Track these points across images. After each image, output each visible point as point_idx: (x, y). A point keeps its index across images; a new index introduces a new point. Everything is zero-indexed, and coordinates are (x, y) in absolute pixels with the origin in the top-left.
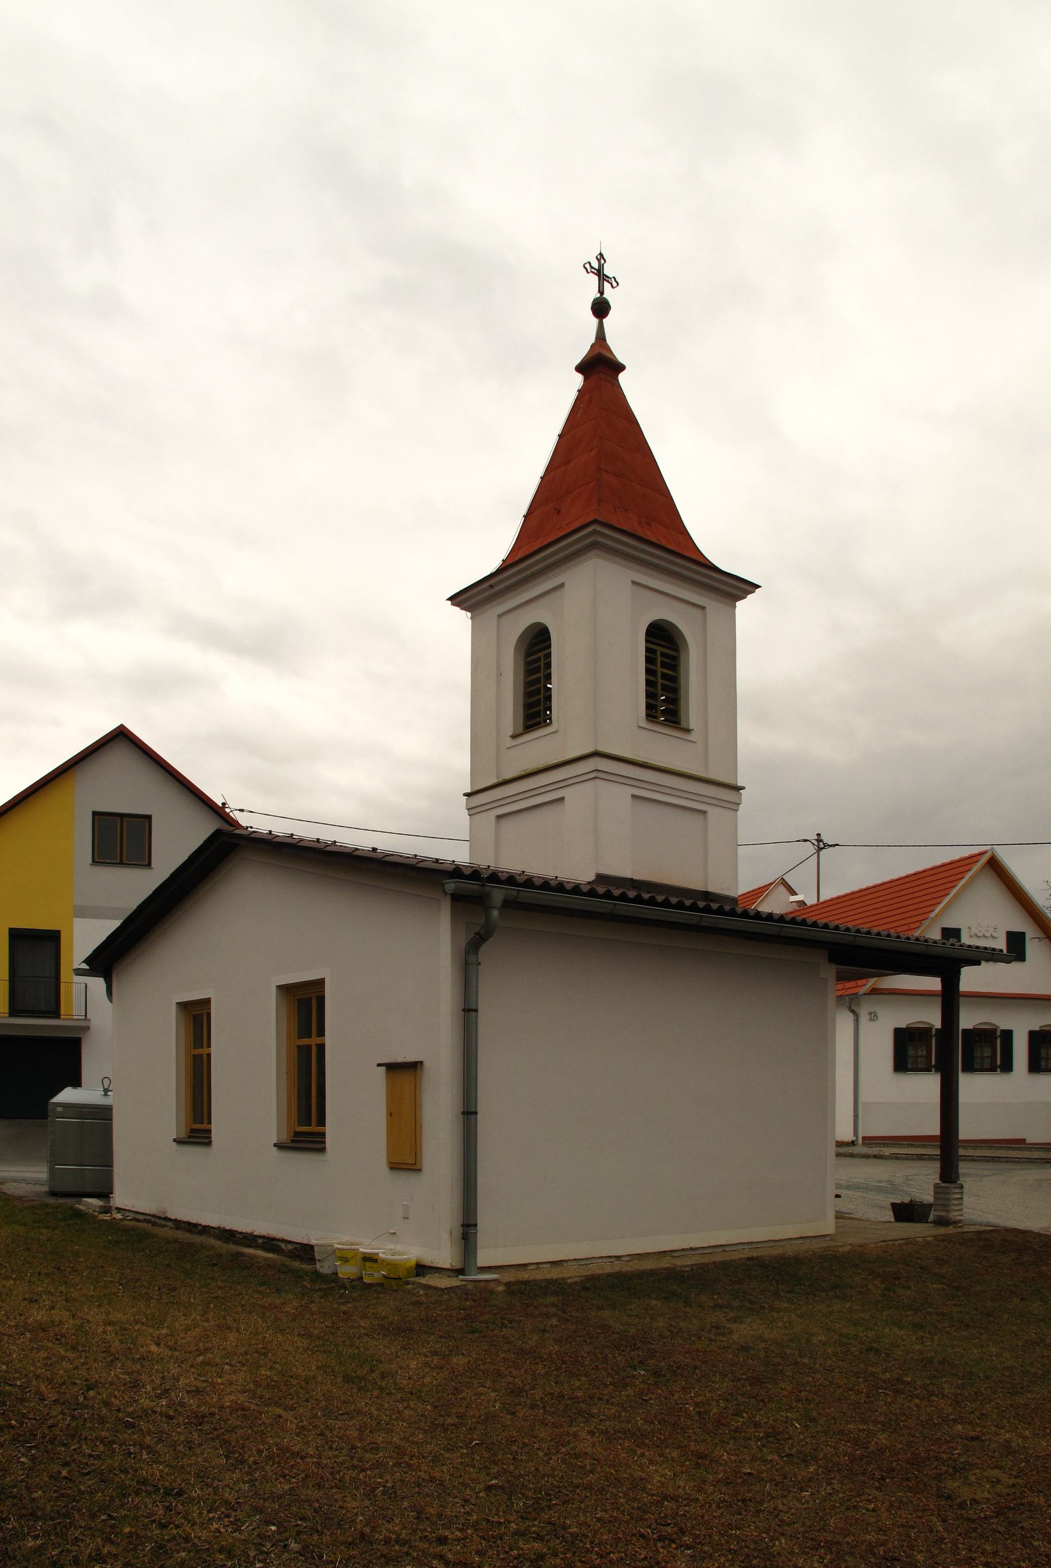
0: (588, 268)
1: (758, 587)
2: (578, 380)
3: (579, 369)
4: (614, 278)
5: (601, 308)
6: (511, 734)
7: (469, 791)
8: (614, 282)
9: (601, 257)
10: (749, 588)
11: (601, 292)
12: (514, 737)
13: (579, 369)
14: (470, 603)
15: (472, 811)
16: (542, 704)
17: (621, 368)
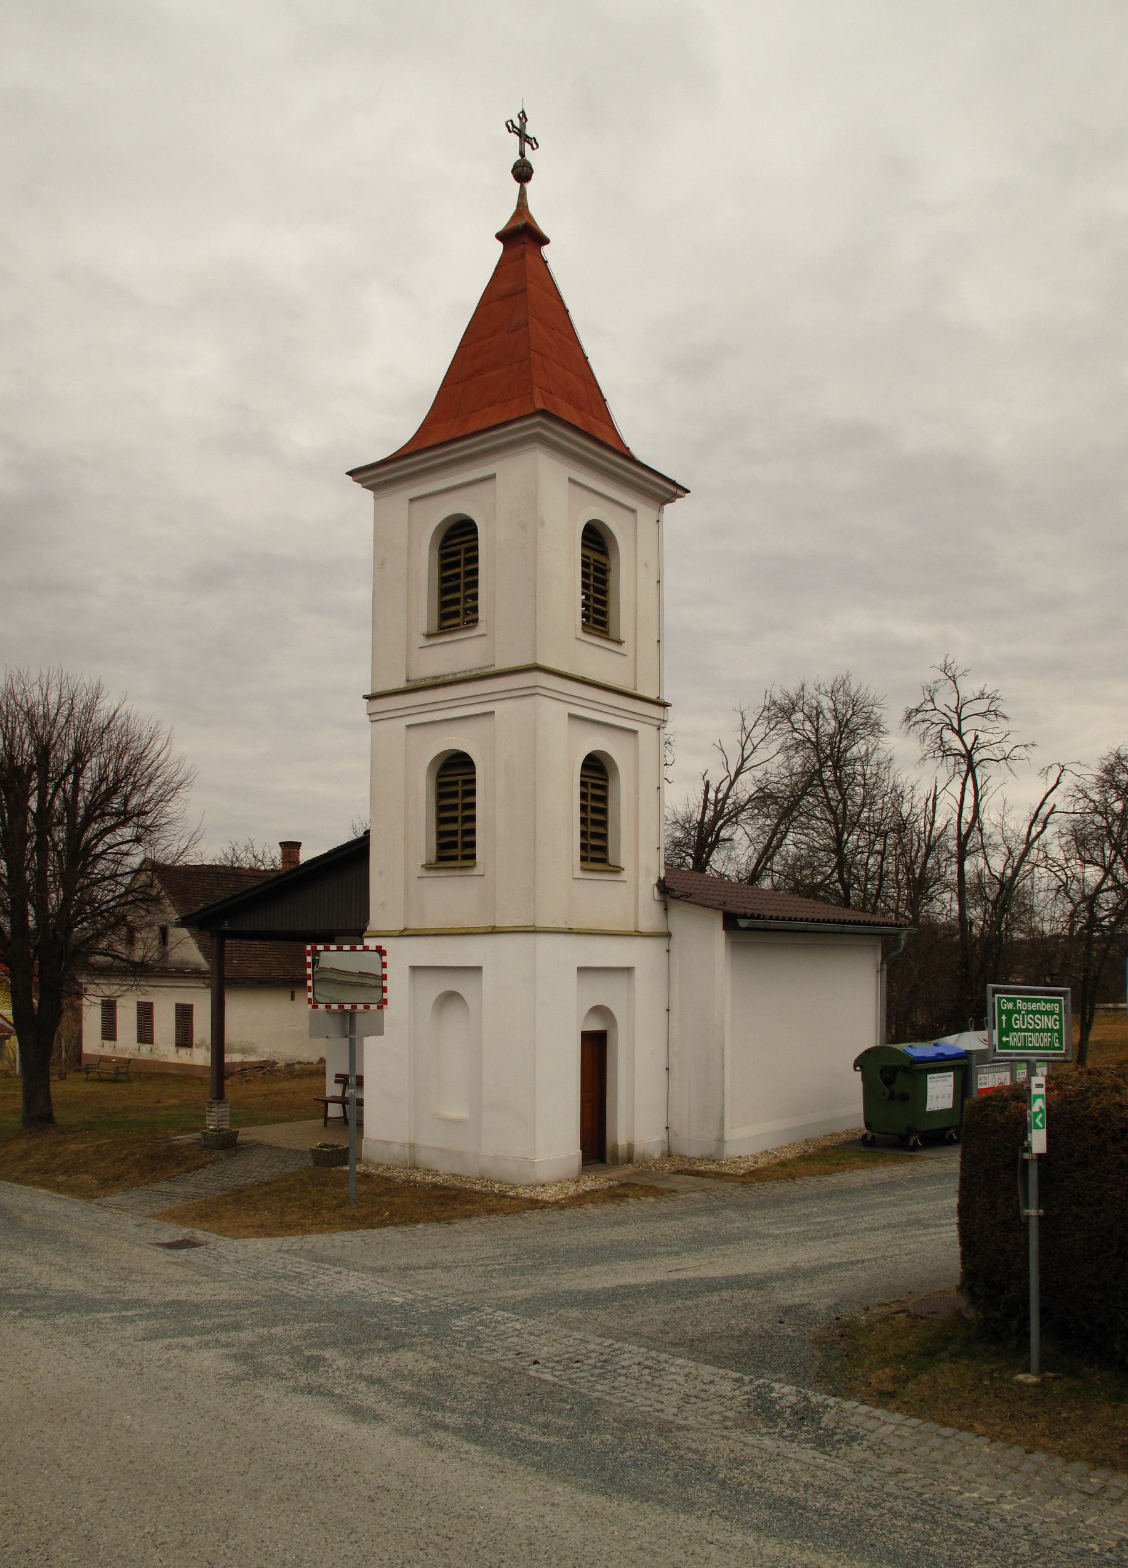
0: (510, 127)
1: (688, 491)
2: (499, 247)
3: (500, 236)
4: (534, 139)
5: (523, 173)
6: (425, 630)
7: (369, 693)
8: (532, 142)
9: (523, 117)
10: (679, 492)
11: (522, 154)
12: (429, 636)
13: (500, 236)
14: (373, 482)
15: (375, 717)
16: (462, 602)
17: (545, 241)
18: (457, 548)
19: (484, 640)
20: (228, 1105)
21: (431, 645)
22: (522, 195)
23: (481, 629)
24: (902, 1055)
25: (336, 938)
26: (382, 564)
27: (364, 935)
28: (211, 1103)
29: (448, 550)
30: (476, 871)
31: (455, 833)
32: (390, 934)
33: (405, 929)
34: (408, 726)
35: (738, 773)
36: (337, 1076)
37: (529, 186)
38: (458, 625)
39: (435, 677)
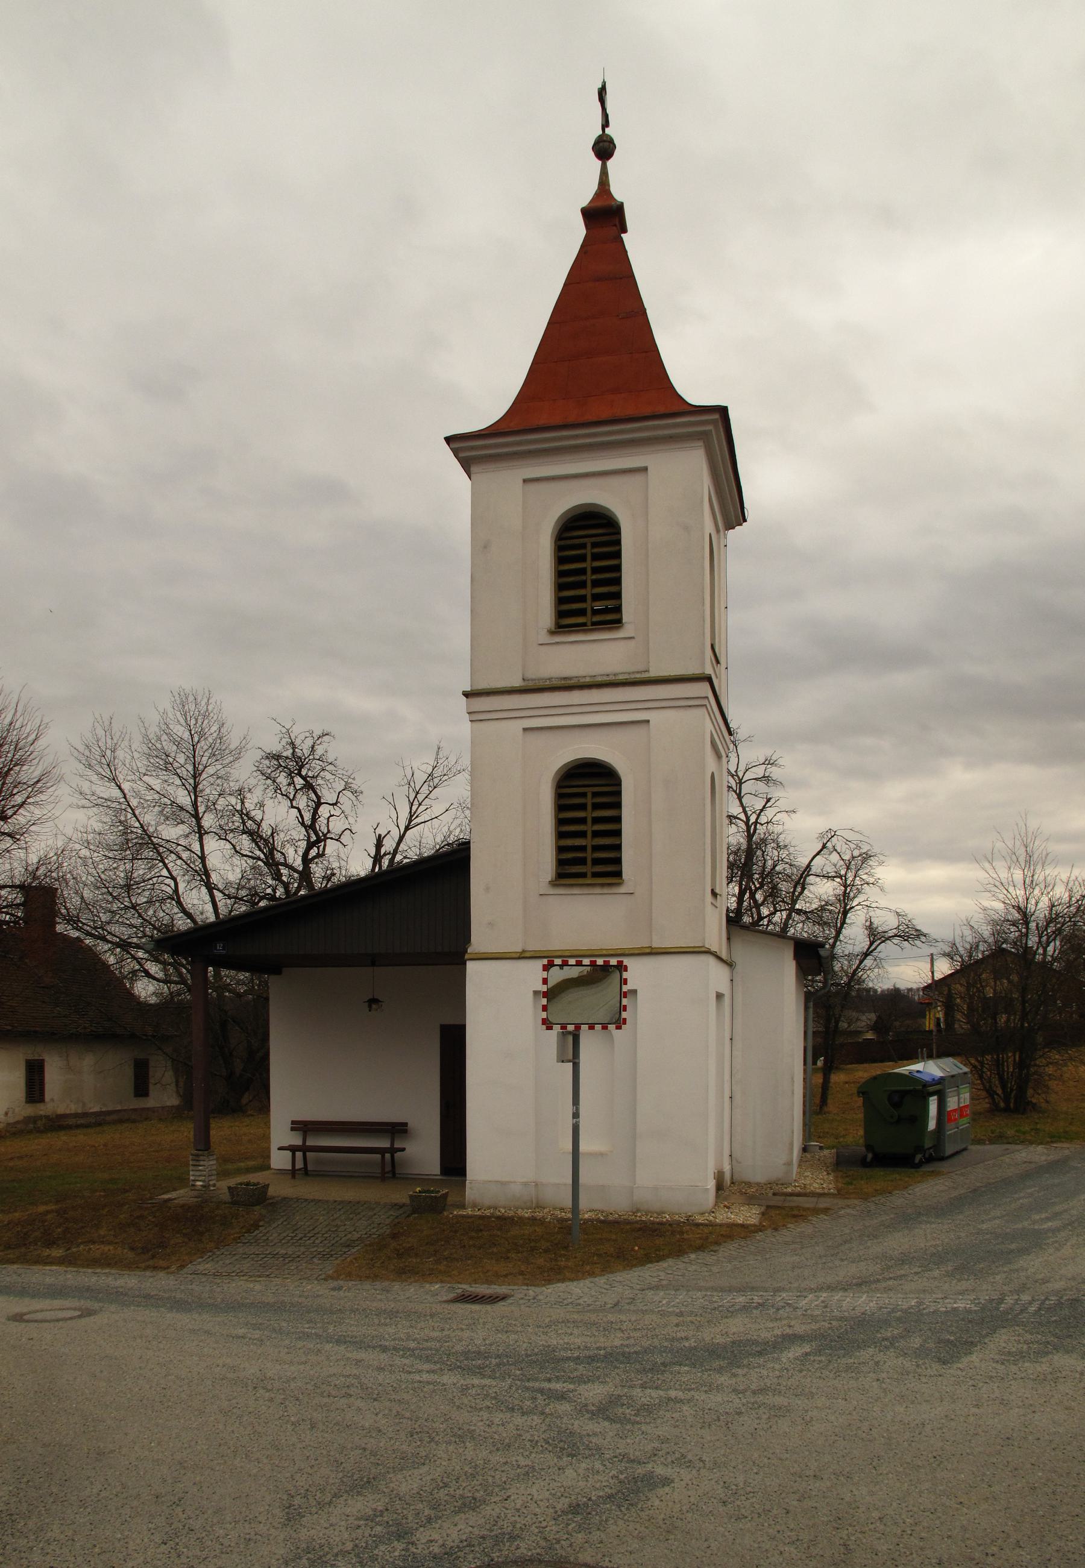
5: (604, 149)
18: (582, 541)
19: (632, 643)
20: (215, 1157)
21: (557, 643)
22: (604, 174)
23: (627, 631)
24: (910, 1078)
25: (284, 969)
26: (485, 547)
27: (466, 957)
28: (197, 1155)
29: (569, 542)
30: (623, 889)
31: (583, 848)
32: (508, 956)
33: (524, 951)
34: (525, 730)
35: (407, 828)
36: (293, 1122)
37: (610, 163)
38: (584, 625)
39: (565, 679)
